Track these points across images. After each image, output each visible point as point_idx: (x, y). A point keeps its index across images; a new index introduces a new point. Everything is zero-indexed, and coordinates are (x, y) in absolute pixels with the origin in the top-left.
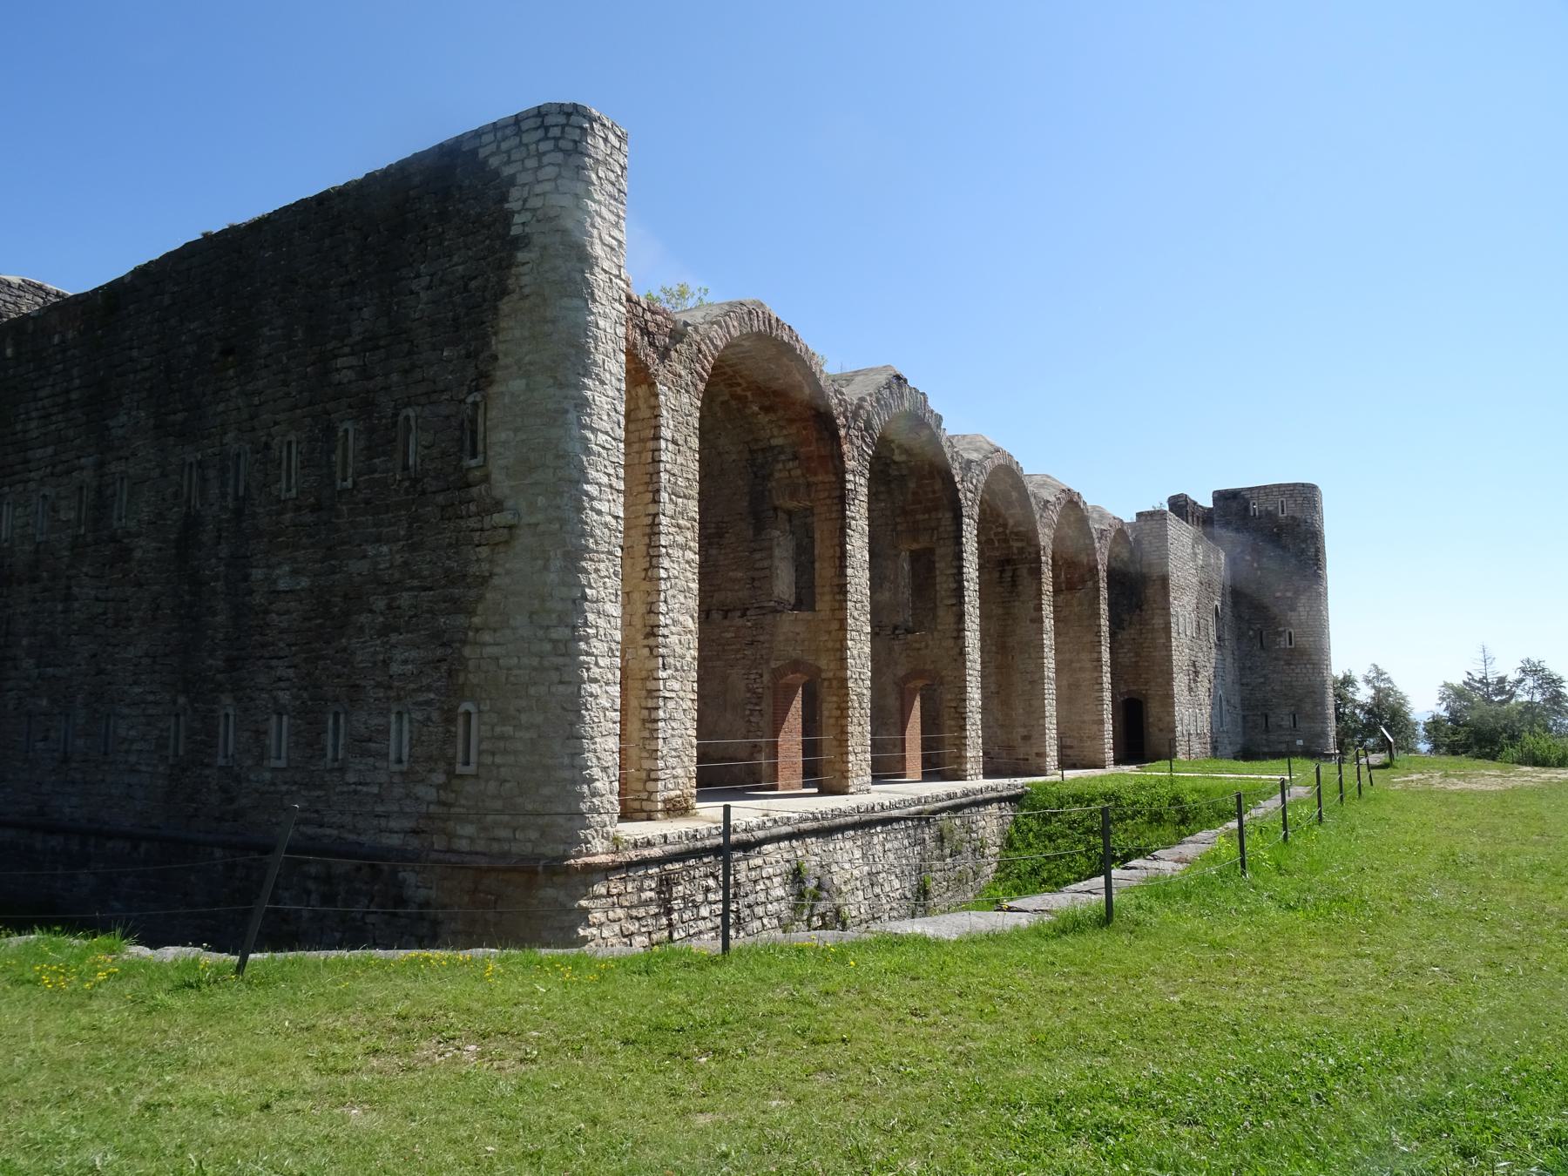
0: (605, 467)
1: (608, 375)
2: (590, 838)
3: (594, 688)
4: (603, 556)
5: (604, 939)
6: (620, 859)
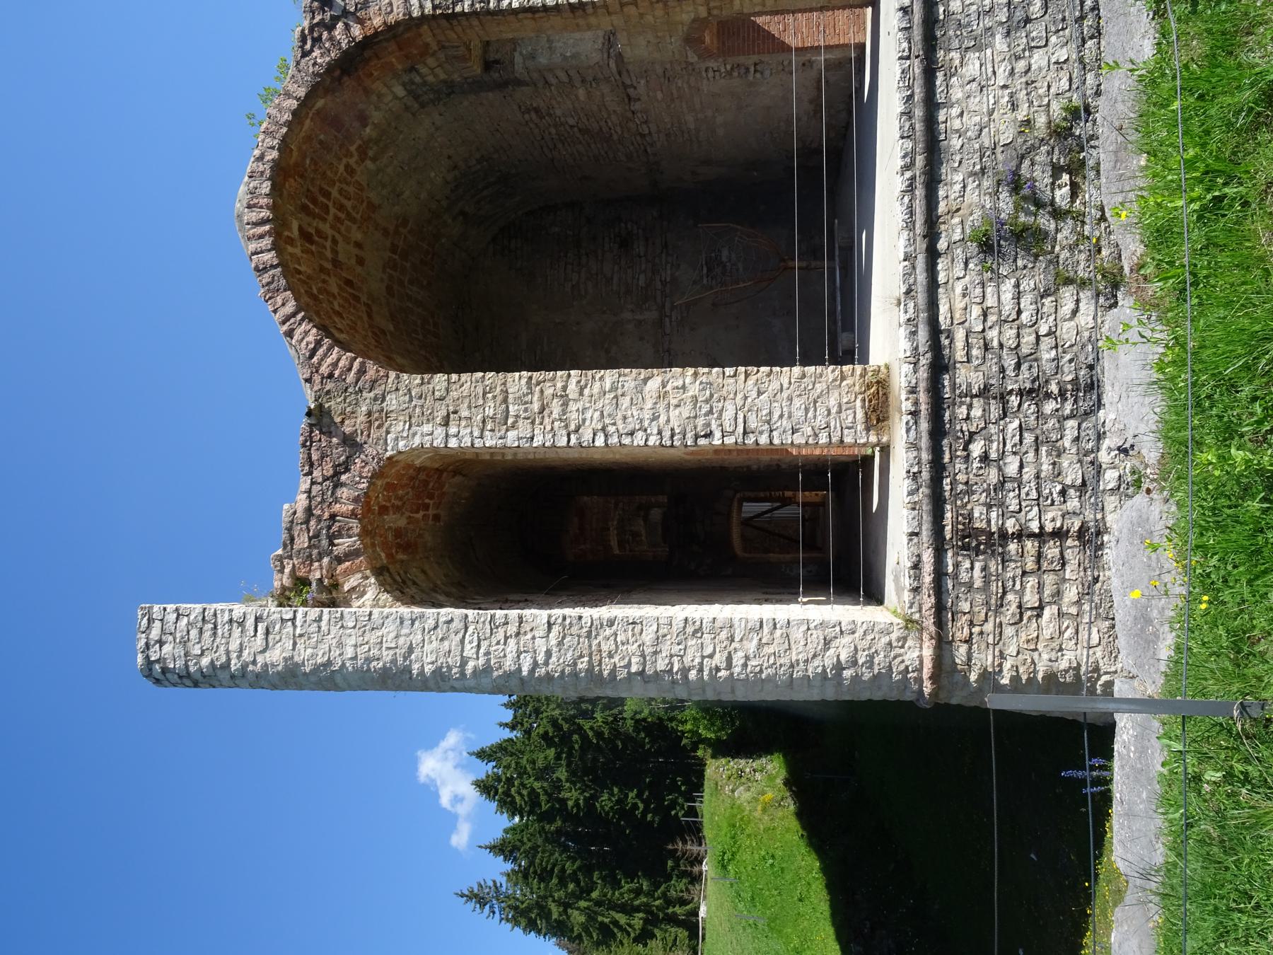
0: (498, 643)
1: (401, 641)
2: (902, 667)
3: (738, 660)
4: (595, 642)
5: (1018, 653)
6: (929, 623)
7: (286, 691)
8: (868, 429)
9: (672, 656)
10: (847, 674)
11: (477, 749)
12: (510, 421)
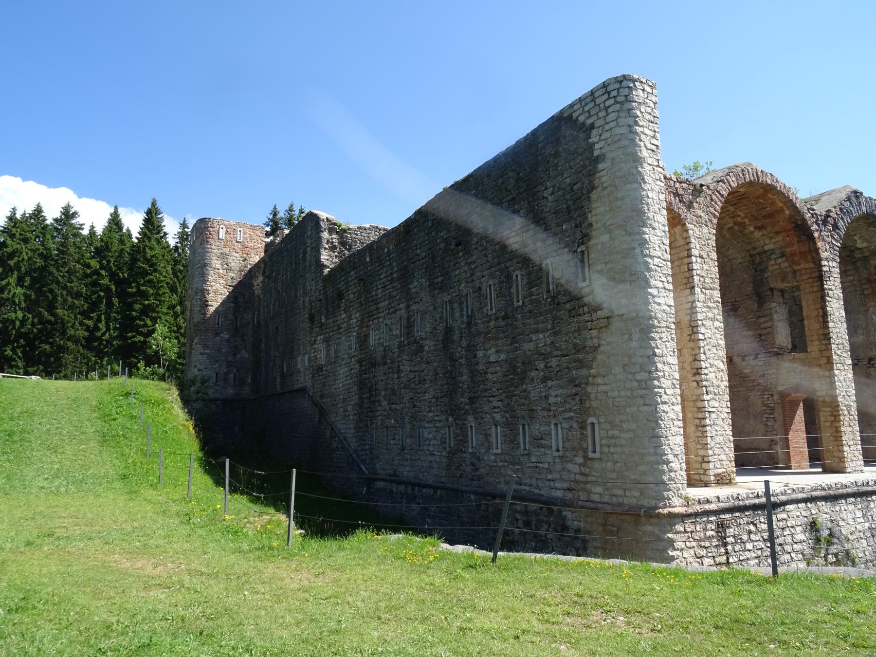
0: (660, 277)
1: (657, 224)
2: (671, 497)
4: (664, 329)
7: (525, 135)
8: (715, 475)
9: (664, 371)
10: (665, 467)
11: (159, 205)
12: (703, 290)
